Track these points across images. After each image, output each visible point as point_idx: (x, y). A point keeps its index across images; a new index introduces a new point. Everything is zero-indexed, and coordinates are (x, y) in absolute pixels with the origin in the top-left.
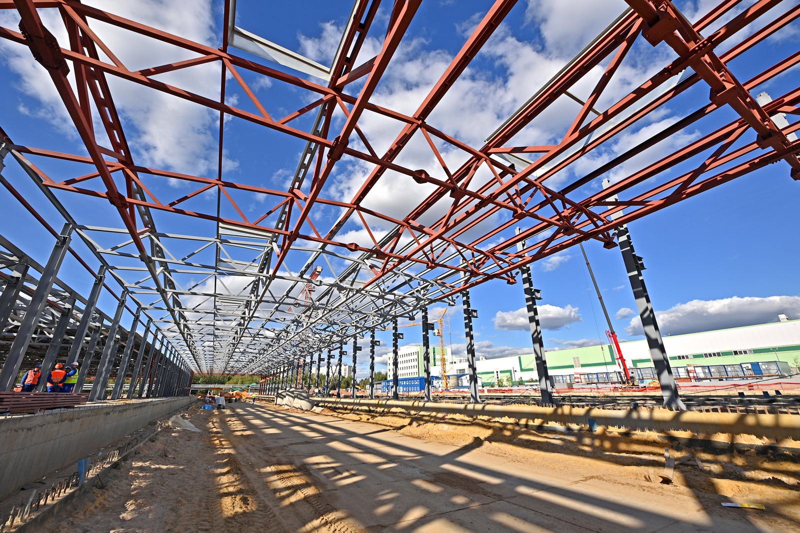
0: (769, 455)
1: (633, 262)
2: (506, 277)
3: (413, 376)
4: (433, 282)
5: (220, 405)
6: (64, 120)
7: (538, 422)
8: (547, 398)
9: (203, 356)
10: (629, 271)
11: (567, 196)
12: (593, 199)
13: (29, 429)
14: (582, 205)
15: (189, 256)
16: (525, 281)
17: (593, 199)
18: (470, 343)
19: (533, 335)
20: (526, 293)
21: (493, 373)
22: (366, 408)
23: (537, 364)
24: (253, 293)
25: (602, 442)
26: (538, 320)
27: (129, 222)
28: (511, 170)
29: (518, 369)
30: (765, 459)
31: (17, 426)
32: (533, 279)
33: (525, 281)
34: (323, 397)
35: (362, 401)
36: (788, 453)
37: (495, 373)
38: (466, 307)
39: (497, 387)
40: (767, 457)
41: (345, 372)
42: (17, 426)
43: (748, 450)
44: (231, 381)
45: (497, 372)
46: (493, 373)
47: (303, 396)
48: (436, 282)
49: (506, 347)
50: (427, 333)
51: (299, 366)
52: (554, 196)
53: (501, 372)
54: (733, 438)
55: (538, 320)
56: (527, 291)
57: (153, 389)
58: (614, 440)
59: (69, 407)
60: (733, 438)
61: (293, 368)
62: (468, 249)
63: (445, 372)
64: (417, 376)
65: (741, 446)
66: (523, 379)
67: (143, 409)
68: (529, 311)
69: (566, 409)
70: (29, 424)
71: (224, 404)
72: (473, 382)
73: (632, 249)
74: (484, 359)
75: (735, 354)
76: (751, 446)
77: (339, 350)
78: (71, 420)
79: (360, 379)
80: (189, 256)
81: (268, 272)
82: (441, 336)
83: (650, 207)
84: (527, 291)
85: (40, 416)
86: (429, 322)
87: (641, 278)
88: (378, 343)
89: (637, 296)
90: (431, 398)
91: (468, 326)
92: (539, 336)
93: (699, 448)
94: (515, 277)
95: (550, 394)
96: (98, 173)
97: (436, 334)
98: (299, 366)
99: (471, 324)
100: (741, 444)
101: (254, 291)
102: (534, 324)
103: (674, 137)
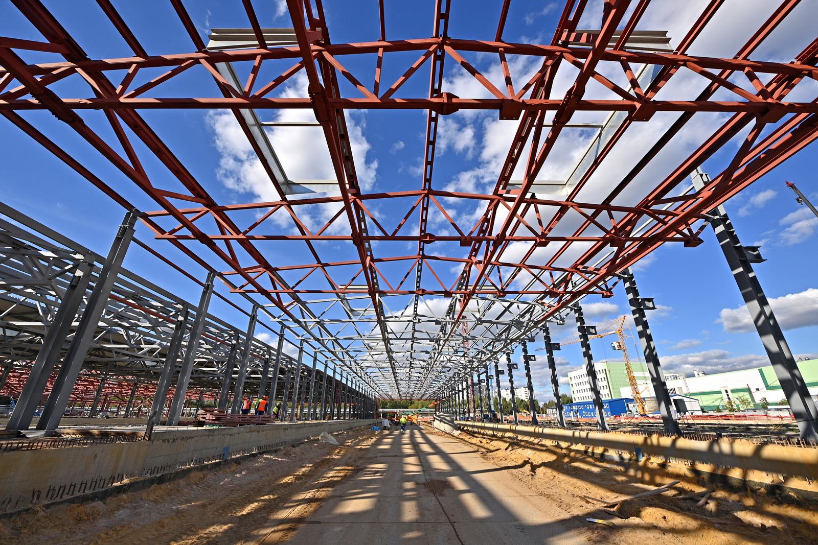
0: (777, 496)
1: (740, 256)
2: (598, 290)
3: (588, 400)
4: (535, 303)
5: (385, 427)
6: (350, 130)
7: (599, 450)
8: (671, 427)
9: (381, 385)
10: (733, 269)
11: (612, 203)
12: (650, 198)
13: (231, 435)
14: (640, 207)
15: (321, 315)
16: (628, 291)
17: (650, 198)
18: (649, 346)
19: (645, 353)
20: (631, 305)
21: (720, 392)
22: (490, 432)
23: (654, 386)
24: (449, 316)
25: (643, 474)
26: (650, 335)
27: (507, 166)
28: (533, 200)
29: (761, 385)
30: (774, 500)
31: (224, 432)
32: (638, 287)
33: (628, 291)
34: (474, 421)
35: (547, 431)
36: (792, 494)
37: (724, 392)
38: (631, 296)
39: (726, 412)
40: (776, 498)
41: (506, 395)
42: (224, 432)
43: (759, 489)
44: (413, 405)
45: (727, 392)
46: (720, 392)
47: (447, 420)
48: (537, 302)
49: (752, 356)
50: (551, 354)
51: (459, 391)
52: (598, 209)
53: (733, 391)
54: (745, 474)
55: (650, 335)
56: (632, 302)
57: (328, 412)
58: (653, 472)
59: (263, 424)
60: (745, 474)
61: (456, 393)
62: (545, 270)
63: (637, 393)
64: (610, 398)
65: (753, 484)
66: (769, 400)
67: (319, 427)
68: (637, 325)
69: (725, 445)
70: (230, 432)
71: (389, 426)
72: (663, 404)
73: (735, 239)
74: (701, 374)
75: (674, 379)
76: (761, 484)
77: (485, 374)
78: (258, 432)
79: (543, 403)
80: (321, 315)
81: (466, 289)
82: (624, 350)
83: (701, 200)
84: (632, 302)
85: (235, 430)
86: (552, 342)
87: (751, 275)
88: (515, 366)
89: (747, 298)
90: (607, 427)
91: (585, 345)
92: (654, 353)
93: (720, 485)
94: (611, 289)
95: (676, 424)
96: (247, 282)
97: (617, 348)
98: (459, 391)
99: (588, 343)
100: (753, 482)
101: (450, 313)
102: (644, 339)
103: (722, 115)
